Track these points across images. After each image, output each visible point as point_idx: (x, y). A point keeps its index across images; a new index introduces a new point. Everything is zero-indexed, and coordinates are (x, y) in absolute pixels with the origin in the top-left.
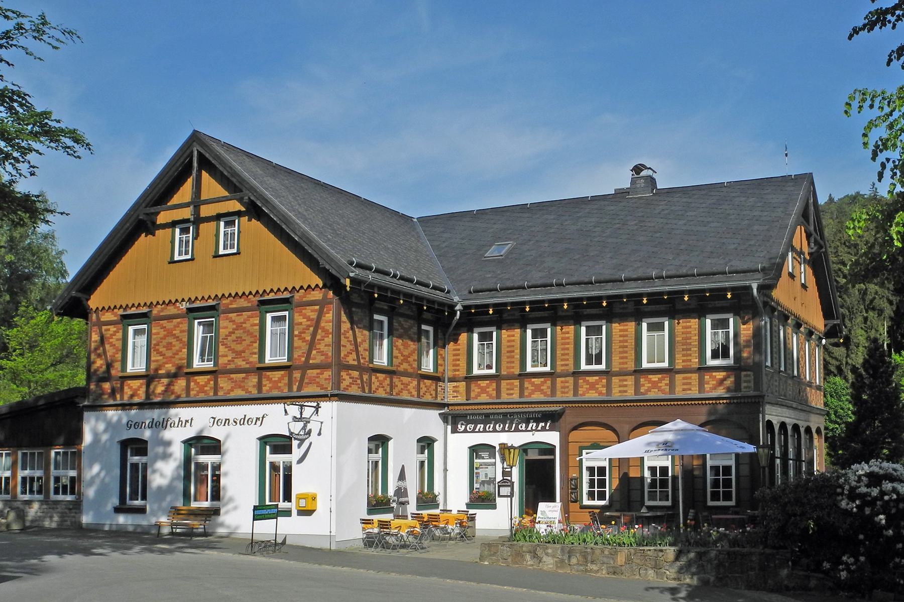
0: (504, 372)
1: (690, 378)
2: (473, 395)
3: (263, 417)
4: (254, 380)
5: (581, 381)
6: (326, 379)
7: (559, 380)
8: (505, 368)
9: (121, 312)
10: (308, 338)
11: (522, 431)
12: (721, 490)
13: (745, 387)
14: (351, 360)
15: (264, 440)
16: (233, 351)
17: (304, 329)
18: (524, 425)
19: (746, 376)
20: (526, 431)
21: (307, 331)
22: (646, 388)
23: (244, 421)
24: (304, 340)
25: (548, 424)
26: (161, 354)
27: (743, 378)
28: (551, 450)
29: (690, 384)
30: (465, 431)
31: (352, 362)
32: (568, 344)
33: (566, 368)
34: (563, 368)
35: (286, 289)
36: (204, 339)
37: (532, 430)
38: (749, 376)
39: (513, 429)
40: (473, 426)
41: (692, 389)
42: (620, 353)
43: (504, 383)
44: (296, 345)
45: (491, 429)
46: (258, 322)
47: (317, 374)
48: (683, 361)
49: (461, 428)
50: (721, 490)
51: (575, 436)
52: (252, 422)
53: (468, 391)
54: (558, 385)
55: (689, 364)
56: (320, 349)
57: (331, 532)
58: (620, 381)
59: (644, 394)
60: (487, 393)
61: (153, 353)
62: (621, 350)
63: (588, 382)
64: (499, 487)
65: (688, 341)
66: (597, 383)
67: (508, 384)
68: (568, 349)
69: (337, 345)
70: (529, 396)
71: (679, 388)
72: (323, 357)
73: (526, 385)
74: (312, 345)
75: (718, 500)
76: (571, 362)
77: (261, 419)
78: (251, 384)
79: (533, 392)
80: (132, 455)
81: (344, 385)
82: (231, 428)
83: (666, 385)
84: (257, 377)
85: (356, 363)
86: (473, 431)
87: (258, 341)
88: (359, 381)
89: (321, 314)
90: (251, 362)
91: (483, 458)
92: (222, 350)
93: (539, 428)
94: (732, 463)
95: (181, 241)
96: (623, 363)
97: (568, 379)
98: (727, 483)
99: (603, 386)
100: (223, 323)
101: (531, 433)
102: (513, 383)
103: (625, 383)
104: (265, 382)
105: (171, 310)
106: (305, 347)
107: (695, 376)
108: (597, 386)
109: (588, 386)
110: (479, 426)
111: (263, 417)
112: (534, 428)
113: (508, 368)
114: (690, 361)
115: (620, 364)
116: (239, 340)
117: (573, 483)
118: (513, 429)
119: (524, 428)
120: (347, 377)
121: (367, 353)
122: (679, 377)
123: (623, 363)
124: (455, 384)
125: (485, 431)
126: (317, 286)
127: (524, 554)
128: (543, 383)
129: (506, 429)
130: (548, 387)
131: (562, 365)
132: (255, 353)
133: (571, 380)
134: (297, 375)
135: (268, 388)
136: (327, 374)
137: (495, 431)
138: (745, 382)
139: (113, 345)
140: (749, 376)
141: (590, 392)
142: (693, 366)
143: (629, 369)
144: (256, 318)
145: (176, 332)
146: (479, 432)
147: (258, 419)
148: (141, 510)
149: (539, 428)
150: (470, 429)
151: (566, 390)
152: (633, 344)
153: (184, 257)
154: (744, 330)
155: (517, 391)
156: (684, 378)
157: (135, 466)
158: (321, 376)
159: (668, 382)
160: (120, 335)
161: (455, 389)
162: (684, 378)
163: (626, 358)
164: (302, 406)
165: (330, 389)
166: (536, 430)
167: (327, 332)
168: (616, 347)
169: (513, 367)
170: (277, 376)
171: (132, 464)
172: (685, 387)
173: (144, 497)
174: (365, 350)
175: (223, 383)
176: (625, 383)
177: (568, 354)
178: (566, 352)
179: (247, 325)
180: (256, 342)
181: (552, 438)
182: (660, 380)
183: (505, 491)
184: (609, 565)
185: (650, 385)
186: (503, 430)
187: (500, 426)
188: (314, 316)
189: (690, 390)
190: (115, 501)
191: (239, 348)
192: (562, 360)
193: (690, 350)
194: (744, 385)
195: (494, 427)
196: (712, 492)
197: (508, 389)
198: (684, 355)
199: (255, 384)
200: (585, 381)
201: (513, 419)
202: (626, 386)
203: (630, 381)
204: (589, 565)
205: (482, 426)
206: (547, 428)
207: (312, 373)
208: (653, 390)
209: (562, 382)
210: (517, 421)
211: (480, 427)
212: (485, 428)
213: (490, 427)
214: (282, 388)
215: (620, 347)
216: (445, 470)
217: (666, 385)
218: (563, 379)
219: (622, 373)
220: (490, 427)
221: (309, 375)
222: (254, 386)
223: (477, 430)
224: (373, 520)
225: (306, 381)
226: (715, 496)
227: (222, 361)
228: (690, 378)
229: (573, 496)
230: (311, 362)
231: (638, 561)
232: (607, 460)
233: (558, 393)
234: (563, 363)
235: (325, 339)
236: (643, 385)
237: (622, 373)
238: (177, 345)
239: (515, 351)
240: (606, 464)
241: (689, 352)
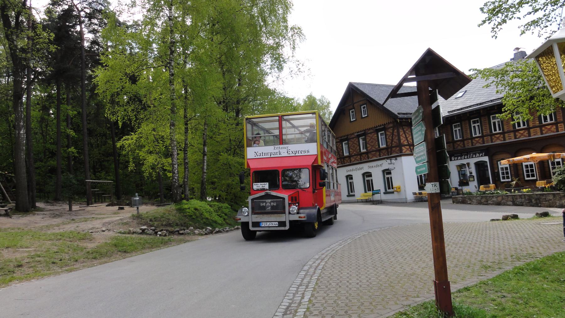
0: (484, 134)
1: (536, 130)
2: (455, 147)
4: (359, 157)
5: (517, 133)
7: (485, 138)
9: (340, 139)
10: (391, 138)
13: (561, 130)
14: (406, 143)
15: (384, 171)
16: (371, 145)
19: (560, 125)
20: (476, 157)
23: (377, 166)
24: (390, 139)
25: (484, 153)
26: (352, 149)
27: (559, 127)
30: (455, 160)
31: (405, 144)
32: (487, 124)
34: (486, 133)
35: (382, 124)
36: (363, 143)
37: (478, 157)
38: (562, 125)
43: (466, 142)
44: (388, 141)
48: (533, 124)
49: (453, 159)
50: (505, 175)
53: (454, 146)
58: (508, 135)
60: (499, 139)
61: (350, 149)
63: (496, 137)
64: (469, 178)
66: (499, 137)
68: (486, 126)
69: (399, 139)
70: (475, 145)
71: (507, 138)
74: (392, 140)
75: (505, 179)
79: (476, 143)
80: (366, 177)
81: (404, 151)
82: (374, 169)
85: (407, 144)
86: (457, 160)
88: (409, 149)
89: (393, 130)
92: (368, 145)
95: (363, 110)
96: (508, 128)
98: (507, 173)
99: (502, 138)
100: (367, 138)
102: (468, 142)
103: (510, 135)
104: (345, 161)
105: (353, 136)
106: (390, 141)
107: (538, 129)
114: (535, 123)
115: (507, 128)
116: (372, 142)
120: (405, 149)
121: (411, 140)
123: (508, 128)
125: (461, 159)
131: (485, 132)
133: (489, 137)
134: (390, 150)
136: (398, 148)
137: (465, 158)
138: (560, 128)
139: (339, 148)
140: (562, 125)
145: (355, 142)
146: (459, 159)
148: (354, 195)
153: (365, 116)
155: (470, 144)
156: (534, 130)
157: (368, 181)
160: (341, 145)
162: (534, 130)
164: (391, 160)
166: (479, 157)
167: (396, 136)
171: (367, 180)
172: (535, 133)
173: (354, 192)
174: (410, 139)
175: (370, 156)
176: (510, 135)
181: (486, 159)
182: (524, 132)
183: (472, 179)
186: (468, 158)
188: (391, 131)
190: (384, 191)
191: (372, 144)
192: (485, 131)
194: (560, 129)
195: (464, 157)
196: (527, 175)
200: (545, 128)
202: (511, 136)
203: (512, 135)
207: (394, 149)
211: (459, 158)
212: (461, 158)
217: (527, 134)
219: (467, 139)
226: (528, 176)
227: (369, 149)
233: (485, 142)
236: (518, 135)
237: (467, 139)
238: (356, 146)
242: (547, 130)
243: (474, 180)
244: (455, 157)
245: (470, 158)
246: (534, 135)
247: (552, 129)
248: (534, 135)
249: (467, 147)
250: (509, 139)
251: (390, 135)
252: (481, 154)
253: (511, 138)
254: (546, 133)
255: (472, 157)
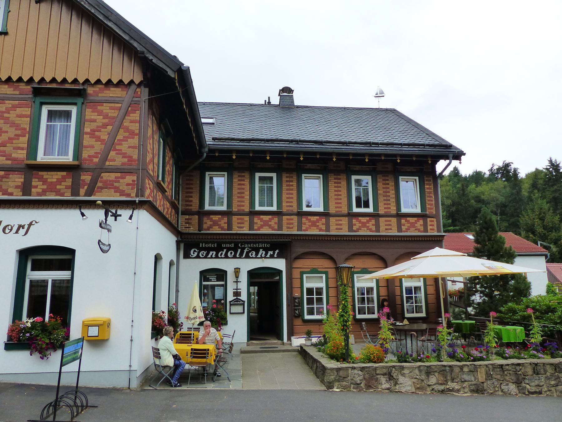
1: (390, 221)
2: (205, 226)
3: (30, 224)
6: (128, 185)
8: (236, 206)
11: (253, 258)
12: (315, 306)
13: (431, 229)
17: (98, 127)
18: (254, 252)
19: (431, 221)
20: (256, 258)
21: (103, 130)
22: (358, 227)
25: (277, 251)
27: (429, 223)
28: (279, 272)
29: (390, 225)
30: (198, 257)
32: (292, 190)
33: (291, 208)
34: (288, 208)
37: (261, 257)
38: (433, 221)
39: (244, 256)
40: (205, 253)
41: (392, 229)
42: (336, 199)
43: (235, 218)
44: (85, 143)
45: (223, 256)
46: (29, 113)
47: (116, 178)
48: (385, 208)
50: (315, 306)
51: (301, 264)
52: (11, 230)
54: (283, 221)
55: (389, 210)
56: (121, 150)
57: (130, 366)
59: (356, 232)
62: (336, 197)
65: (388, 194)
66: (318, 221)
67: (238, 219)
72: (126, 160)
73: (256, 220)
76: (295, 205)
77: (26, 227)
78: (11, 184)
83: (373, 225)
84: (23, 176)
86: (206, 257)
87: (27, 135)
90: (15, 159)
91: (211, 281)
93: (268, 256)
94: (421, 284)
97: (292, 217)
99: (323, 224)
101: (261, 260)
102: (243, 219)
103: (340, 222)
104: (35, 182)
108: (317, 224)
109: (310, 224)
110: (211, 253)
111: (30, 224)
112: (263, 256)
113: (238, 206)
117: (297, 301)
118: (244, 256)
119: (254, 256)
122: (382, 220)
124: (187, 217)
125: (217, 257)
126: (132, 82)
127: (379, 376)
128: (270, 220)
129: (238, 256)
130: (275, 223)
131: (287, 206)
132: (22, 149)
133: (295, 218)
134: (86, 178)
135: (41, 191)
136: (129, 179)
141: (312, 228)
142: (392, 212)
143: (343, 212)
144: (27, 109)
146: (211, 257)
147: (21, 227)
149: (268, 256)
150: (202, 255)
151: (291, 226)
152: (346, 193)
154: (428, 188)
155: (247, 225)
156: (386, 221)
158: (121, 181)
159: (374, 223)
161: (187, 221)
162: (386, 221)
163: (340, 203)
165: (133, 195)
166: (265, 257)
168: (332, 195)
169: (243, 206)
170: (57, 177)
172: (387, 227)
176: (340, 222)
177: (292, 198)
178: (291, 196)
179: (12, 116)
180: (25, 136)
181: (280, 264)
184: (470, 383)
185: (360, 225)
186: (235, 257)
187: (231, 253)
189: (391, 229)
192: (287, 202)
193: (389, 200)
194: (429, 227)
197: (238, 223)
198: (385, 204)
199: (20, 184)
200: (307, 219)
201: (244, 248)
203: (345, 221)
204: (449, 383)
205: (215, 253)
206: (275, 256)
208: (362, 229)
209: (288, 219)
210: (248, 249)
213: (222, 253)
214: (62, 191)
215: (336, 195)
216: (177, 291)
217: (373, 225)
218: (430, 219)
220: (222, 253)
221: (105, 178)
222: (17, 187)
223: (209, 256)
224: (208, 350)
225: (99, 184)
228: (390, 221)
229: (297, 312)
230: (107, 163)
231: (499, 377)
232: (375, 280)
233: (284, 228)
234: (288, 204)
235: (129, 140)
239: (245, 193)
240: (373, 285)
241: (388, 202)
242: (409, 225)
243: (244, 313)
244: (201, 249)
245: (240, 258)
246: (386, 229)
247: (272, 223)
248: (386, 229)
249: (236, 230)
250: (337, 229)
251: (105, 126)
252: (270, 253)
253: (341, 229)
254: (407, 230)
255: (247, 257)
